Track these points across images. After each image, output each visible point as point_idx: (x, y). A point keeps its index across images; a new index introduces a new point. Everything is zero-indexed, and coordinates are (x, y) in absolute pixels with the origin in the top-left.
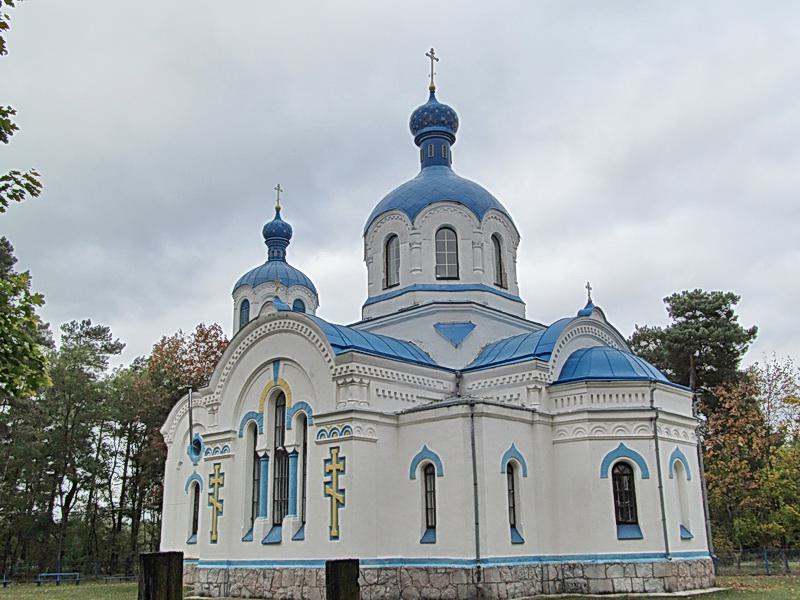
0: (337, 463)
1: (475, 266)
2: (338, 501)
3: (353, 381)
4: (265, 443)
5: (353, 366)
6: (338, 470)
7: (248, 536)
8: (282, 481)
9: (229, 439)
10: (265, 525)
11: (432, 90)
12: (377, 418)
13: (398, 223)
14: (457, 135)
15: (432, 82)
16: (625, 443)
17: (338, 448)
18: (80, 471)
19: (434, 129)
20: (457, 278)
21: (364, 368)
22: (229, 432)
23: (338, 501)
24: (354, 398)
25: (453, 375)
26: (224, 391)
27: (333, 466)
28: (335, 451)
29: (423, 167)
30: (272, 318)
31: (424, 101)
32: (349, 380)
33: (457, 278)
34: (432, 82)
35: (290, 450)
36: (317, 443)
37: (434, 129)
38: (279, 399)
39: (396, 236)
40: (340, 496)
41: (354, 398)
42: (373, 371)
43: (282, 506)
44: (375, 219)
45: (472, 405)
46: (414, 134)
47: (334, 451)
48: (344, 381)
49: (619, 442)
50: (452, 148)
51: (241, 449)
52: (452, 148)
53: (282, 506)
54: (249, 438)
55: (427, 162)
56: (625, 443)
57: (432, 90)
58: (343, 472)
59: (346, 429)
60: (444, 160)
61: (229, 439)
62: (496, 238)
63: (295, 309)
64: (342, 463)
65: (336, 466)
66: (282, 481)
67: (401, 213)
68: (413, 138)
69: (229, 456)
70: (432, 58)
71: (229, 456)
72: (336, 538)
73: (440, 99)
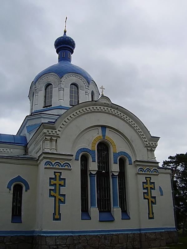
2: (152, 201)
4: (93, 166)
6: (151, 188)
11: (65, 32)
13: (52, 78)
16: (113, 173)
18: (178, 174)
19: (65, 46)
21: (152, 143)
23: (152, 201)
27: (149, 186)
31: (62, 35)
34: (65, 29)
37: (65, 46)
40: (153, 200)
42: (151, 144)
43: (103, 175)
46: (56, 48)
49: (25, 127)
51: (77, 166)
52: (72, 55)
53: (103, 175)
55: (60, 59)
56: (26, 126)
57: (65, 32)
58: (64, 186)
60: (69, 59)
72: (152, 218)
73: (68, 35)
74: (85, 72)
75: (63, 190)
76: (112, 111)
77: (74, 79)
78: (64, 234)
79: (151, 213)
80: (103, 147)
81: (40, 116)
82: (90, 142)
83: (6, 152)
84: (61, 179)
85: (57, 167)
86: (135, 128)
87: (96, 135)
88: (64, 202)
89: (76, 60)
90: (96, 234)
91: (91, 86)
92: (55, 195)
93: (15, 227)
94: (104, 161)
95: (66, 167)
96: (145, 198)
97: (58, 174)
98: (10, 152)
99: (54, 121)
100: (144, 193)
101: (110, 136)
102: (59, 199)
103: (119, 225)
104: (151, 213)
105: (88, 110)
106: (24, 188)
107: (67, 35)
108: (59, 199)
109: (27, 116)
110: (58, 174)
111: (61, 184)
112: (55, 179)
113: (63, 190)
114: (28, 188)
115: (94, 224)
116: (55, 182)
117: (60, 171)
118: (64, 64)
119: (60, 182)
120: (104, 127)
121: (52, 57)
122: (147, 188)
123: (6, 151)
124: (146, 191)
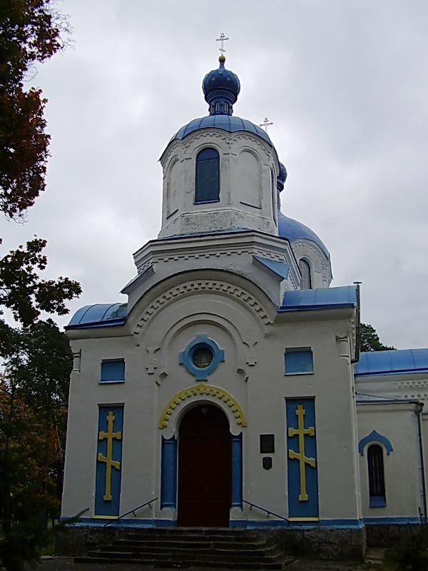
11: (222, 60)
55: (213, 112)
57: (222, 60)
76: (196, 286)
78: (93, 525)
83: (193, 290)
86: (234, 295)
89: (241, 110)
90: (378, 523)
98: (193, 290)
99: (123, 323)
102: (112, 466)
105: (161, 302)
106: (385, 452)
107: (227, 67)
108: (112, 466)
109: (150, 242)
111: (116, 438)
114: (390, 450)
121: (201, 109)
123: (177, 292)
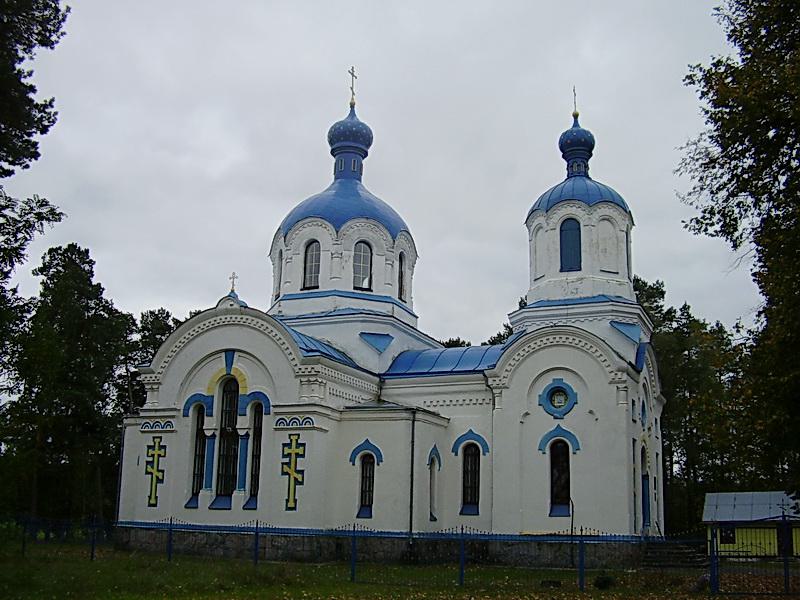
0: (297, 448)
1: (384, 281)
3: (316, 380)
4: (212, 424)
5: (318, 367)
6: (159, 456)
7: (193, 503)
8: (229, 459)
9: (173, 417)
10: (246, 497)
12: (329, 412)
13: (324, 233)
14: (370, 151)
15: (353, 99)
17: (161, 438)
20: (317, 287)
22: (172, 410)
23: (296, 479)
24: (316, 394)
25: (377, 379)
26: (512, 376)
27: (293, 450)
28: (159, 440)
29: (336, 179)
30: (227, 312)
32: (312, 379)
33: (317, 287)
34: (353, 99)
35: (242, 433)
36: (142, 432)
38: (230, 385)
39: (317, 241)
41: (316, 394)
43: (229, 435)
44: (287, 229)
45: (414, 413)
47: (157, 440)
48: (308, 379)
50: (364, 162)
51: (185, 427)
52: (364, 162)
54: (251, 418)
57: (352, 106)
58: (303, 456)
59: (308, 420)
61: (173, 417)
62: (401, 257)
63: (521, 307)
64: (301, 448)
65: (293, 453)
66: (229, 459)
67: (327, 223)
68: (330, 149)
69: (172, 431)
70: (353, 75)
71: (172, 431)
73: (583, 125)
74: (611, 192)
75: (301, 464)
77: (378, 236)
79: (153, 497)
80: (230, 385)
81: (522, 316)
82: (207, 383)
84: (299, 445)
85: (295, 426)
87: (219, 367)
88: (302, 483)
91: (401, 240)
92: (296, 475)
93: (560, 526)
94: (230, 413)
95: (168, 429)
96: (163, 471)
97: (294, 438)
100: (283, 464)
101: (240, 366)
103: (236, 516)
104: (153, 497)
110: (294, 438)
112: (289, 445)
113: (301, 464)
115: (205, 516)
116: (290, 451)
117: (297, 432)
118: (579, 182)
119: (297, 451)
120: (230, 353)
121: (556, 171)
122: (289, 455)
124: (150, 459)
